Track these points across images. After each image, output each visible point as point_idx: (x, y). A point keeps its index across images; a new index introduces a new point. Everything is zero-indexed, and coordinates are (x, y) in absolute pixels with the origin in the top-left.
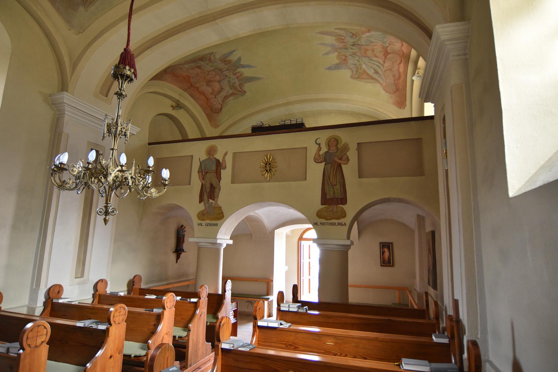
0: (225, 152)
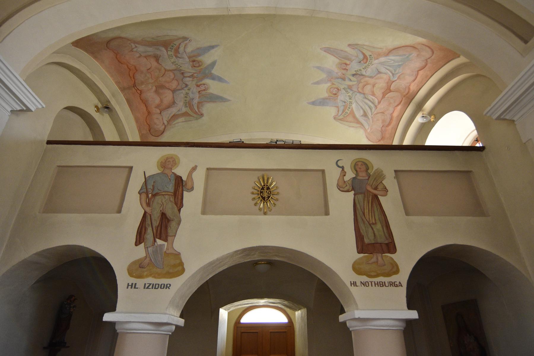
0: (193, 165)
